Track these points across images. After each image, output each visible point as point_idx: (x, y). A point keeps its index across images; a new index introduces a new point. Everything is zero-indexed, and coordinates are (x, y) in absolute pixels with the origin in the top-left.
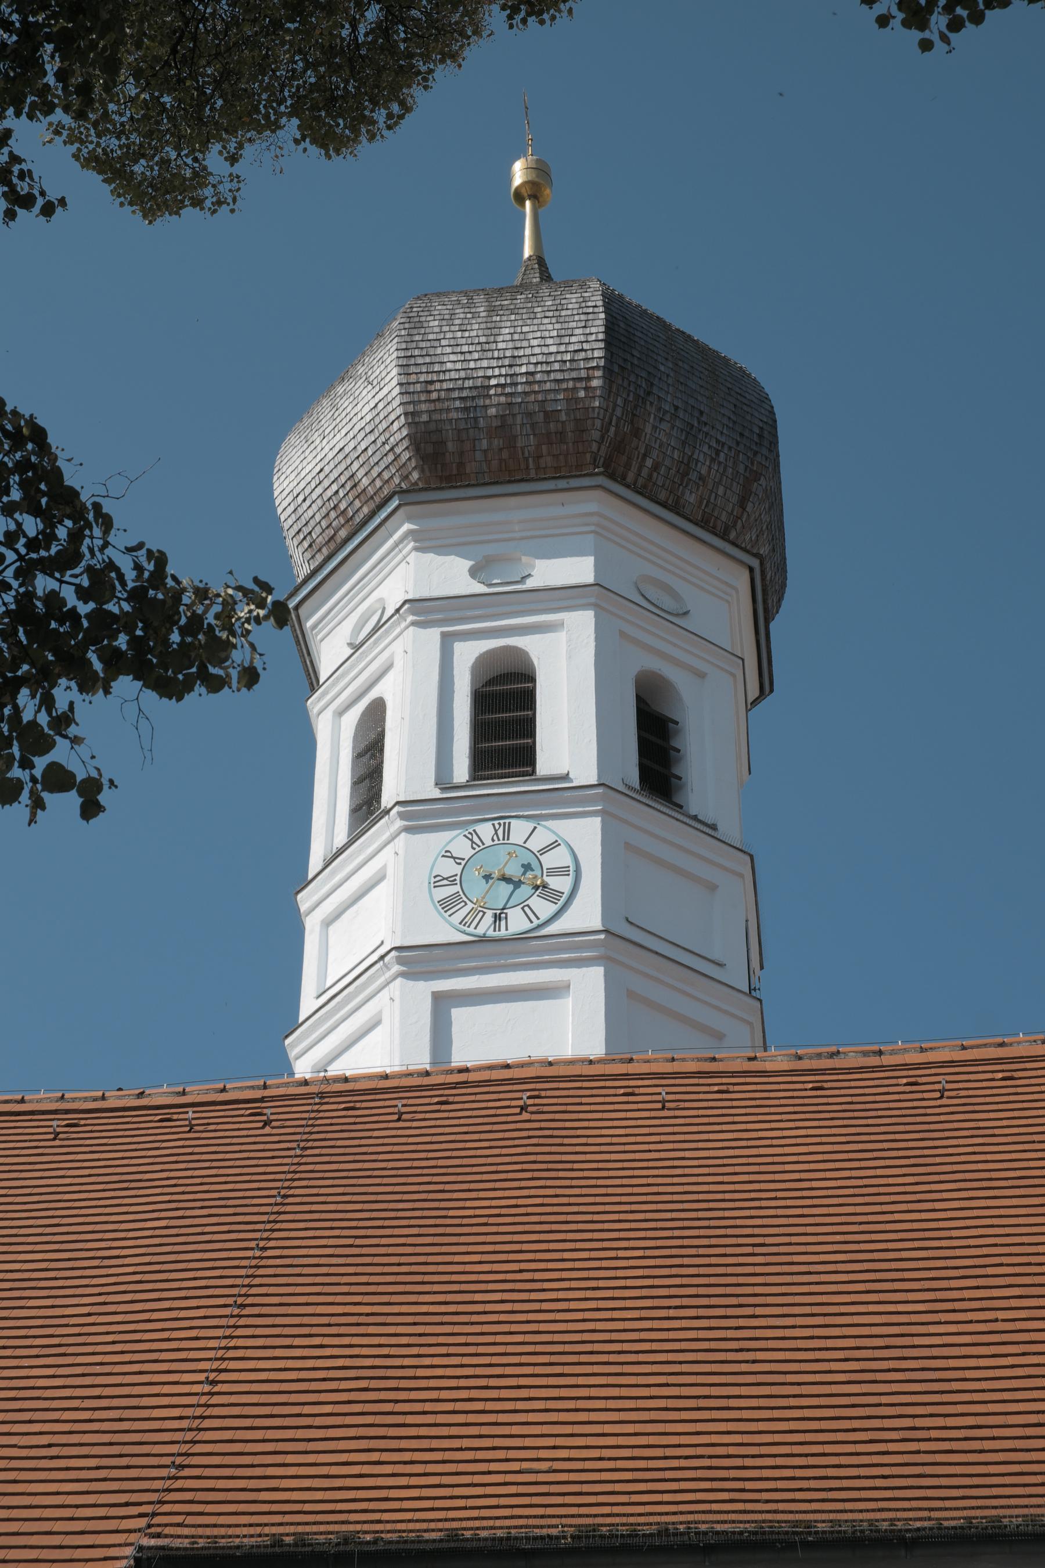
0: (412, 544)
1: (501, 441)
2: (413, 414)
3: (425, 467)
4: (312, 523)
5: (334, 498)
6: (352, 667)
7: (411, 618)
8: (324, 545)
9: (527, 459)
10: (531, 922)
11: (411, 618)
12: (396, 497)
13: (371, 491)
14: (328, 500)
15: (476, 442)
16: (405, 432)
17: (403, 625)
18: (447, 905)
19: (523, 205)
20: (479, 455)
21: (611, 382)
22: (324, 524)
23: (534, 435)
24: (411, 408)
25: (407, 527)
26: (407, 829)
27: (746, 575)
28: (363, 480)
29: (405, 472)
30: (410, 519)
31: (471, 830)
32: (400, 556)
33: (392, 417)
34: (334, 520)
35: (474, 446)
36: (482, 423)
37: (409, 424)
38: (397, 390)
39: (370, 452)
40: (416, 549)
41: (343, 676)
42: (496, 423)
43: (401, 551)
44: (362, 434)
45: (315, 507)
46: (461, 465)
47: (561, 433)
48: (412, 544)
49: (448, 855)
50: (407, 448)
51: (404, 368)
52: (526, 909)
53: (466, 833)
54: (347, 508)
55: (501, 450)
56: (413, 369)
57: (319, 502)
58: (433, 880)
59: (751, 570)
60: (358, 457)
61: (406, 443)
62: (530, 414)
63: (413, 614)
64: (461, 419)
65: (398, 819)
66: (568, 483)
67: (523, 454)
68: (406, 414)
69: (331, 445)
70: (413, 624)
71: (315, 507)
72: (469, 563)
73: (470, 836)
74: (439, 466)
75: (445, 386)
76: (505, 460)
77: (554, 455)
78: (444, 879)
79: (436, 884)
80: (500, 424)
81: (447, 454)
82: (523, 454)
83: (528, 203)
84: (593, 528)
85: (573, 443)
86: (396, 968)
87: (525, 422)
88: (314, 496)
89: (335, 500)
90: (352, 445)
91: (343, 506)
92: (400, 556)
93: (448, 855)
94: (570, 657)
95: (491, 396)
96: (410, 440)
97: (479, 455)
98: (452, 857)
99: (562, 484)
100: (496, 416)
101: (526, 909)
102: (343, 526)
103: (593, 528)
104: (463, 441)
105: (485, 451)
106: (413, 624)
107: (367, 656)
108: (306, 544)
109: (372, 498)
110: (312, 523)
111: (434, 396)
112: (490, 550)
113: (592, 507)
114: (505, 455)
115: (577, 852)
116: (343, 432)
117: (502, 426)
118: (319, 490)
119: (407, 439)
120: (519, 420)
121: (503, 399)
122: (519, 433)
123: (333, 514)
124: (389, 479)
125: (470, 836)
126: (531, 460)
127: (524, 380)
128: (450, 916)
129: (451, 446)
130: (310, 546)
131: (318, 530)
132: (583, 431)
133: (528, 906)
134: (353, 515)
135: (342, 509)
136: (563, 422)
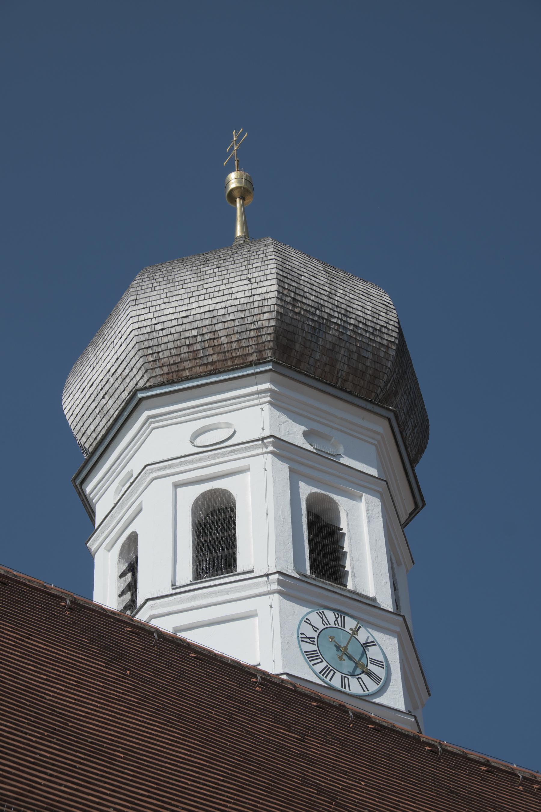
0: (268, 399)
1: (328, 359)
2: (281, 314)
3: (277, 351)
4: (163, 347)
5: (191, 339)
6: (202, 460)
7: (271, 448)
8: (167, 365)
9: (338, 378)
10: (364, 691)
11: (271, 448)
12: (271, 363)
13: (226, 348)
14: (185, 338)
15: (313, 352)
16: (273, 323)
17: (264, 450)
18: (311, 656)
19: (234, 202)
20: (312, 361)
21: (397, 356)
22: (174, 352)
23: (348, 365)
24: (281, 310)
25: (267, 386)
26: (280, 592)
27: (386, 423)
28: (222, 338)
29: (261, 348)
30: (272, 382)
31: (321, 611)
32: (257, 401)
33: (266, 309)
34: (185, 353)
35: (311, 354)
36: (320, 342)
37: (278, 319)
38: (275, 294)
39: (237, 323)
40: (270, 403)
41: (191, 462)
42: (328, 346)
43: (259, 398)
44: (234, 309)
45: (171, 338)
46: (299, 361)
47: (363, 372)
48: (268, 399)
49: (308, 621)
50: (270, 334)
51: (280, 281)
52: (360, 680)
53: (318, 612)
54: (200, 350)
55: (326, 364)
56: (287, 281)
57: (176, 336)
58: (300, 636)
59: (389, 420)
60: (224, 322)
61: (270, 330)
62: (350, 351)
63: (274, 447)
64: (309, 333)
65: (276, 583)
66: (373, 407)
67: (338, 374)
68: (277, 312)
69: (205, 303)
70: (272, 453)
71: (171, 338)
72: (304, 428)
73: (337, 616)
74: (286, 355)
75: (305, 307)
76: (326, 372)
77: (354, 384)
78: (307, 638)
79: (303, 639)
80: (331, 348)
81: (294, 350)
82: (338, 374)
83: (238, 200)
84: (376, 442)
85: (368, 382)
86: (275, 587)
87: (346, 354)
88: (173, 330)
89: (192, 341)
90: (222, 312)
91: (197, 347)
92: (257, 401)
93: (308, 621)
94: (369, 521)
95: (330, 328)
96: (275, 329)
97: (312, 361)
98: (311, 624)
99: (370, 406)
100: (330, 342)
101: (360, 680)
102: (190, 360)
103: (376, 442)
104: (306, 347)
105: (317, 360)
106: (272, 453)
107: (218, 458)
108: (150, 358)
109: (224, 352)
110: (163, 347)
111: (297, 310)
112: (316, 426)
113: (380, 429)
114: (327, 369)
115: (388, 657)
116: (215, 300)
117: (332, 350)
118: (179, 329)
119: (273, 327)
120: (343, 351)
121: (337, 334)
122: (340, 360)
123: (185, 349)
124: (246, 347)
125: (337, 616)
126: (340, 379)
127: (352, 329)
128: (313, 665)
129: (298, 347)
130: (154, 361)
131: (167, 353)
132: (377, 378)
133: (335, 673)
134: (203, 357)
135: (195, 349)
136: (367, 366)
